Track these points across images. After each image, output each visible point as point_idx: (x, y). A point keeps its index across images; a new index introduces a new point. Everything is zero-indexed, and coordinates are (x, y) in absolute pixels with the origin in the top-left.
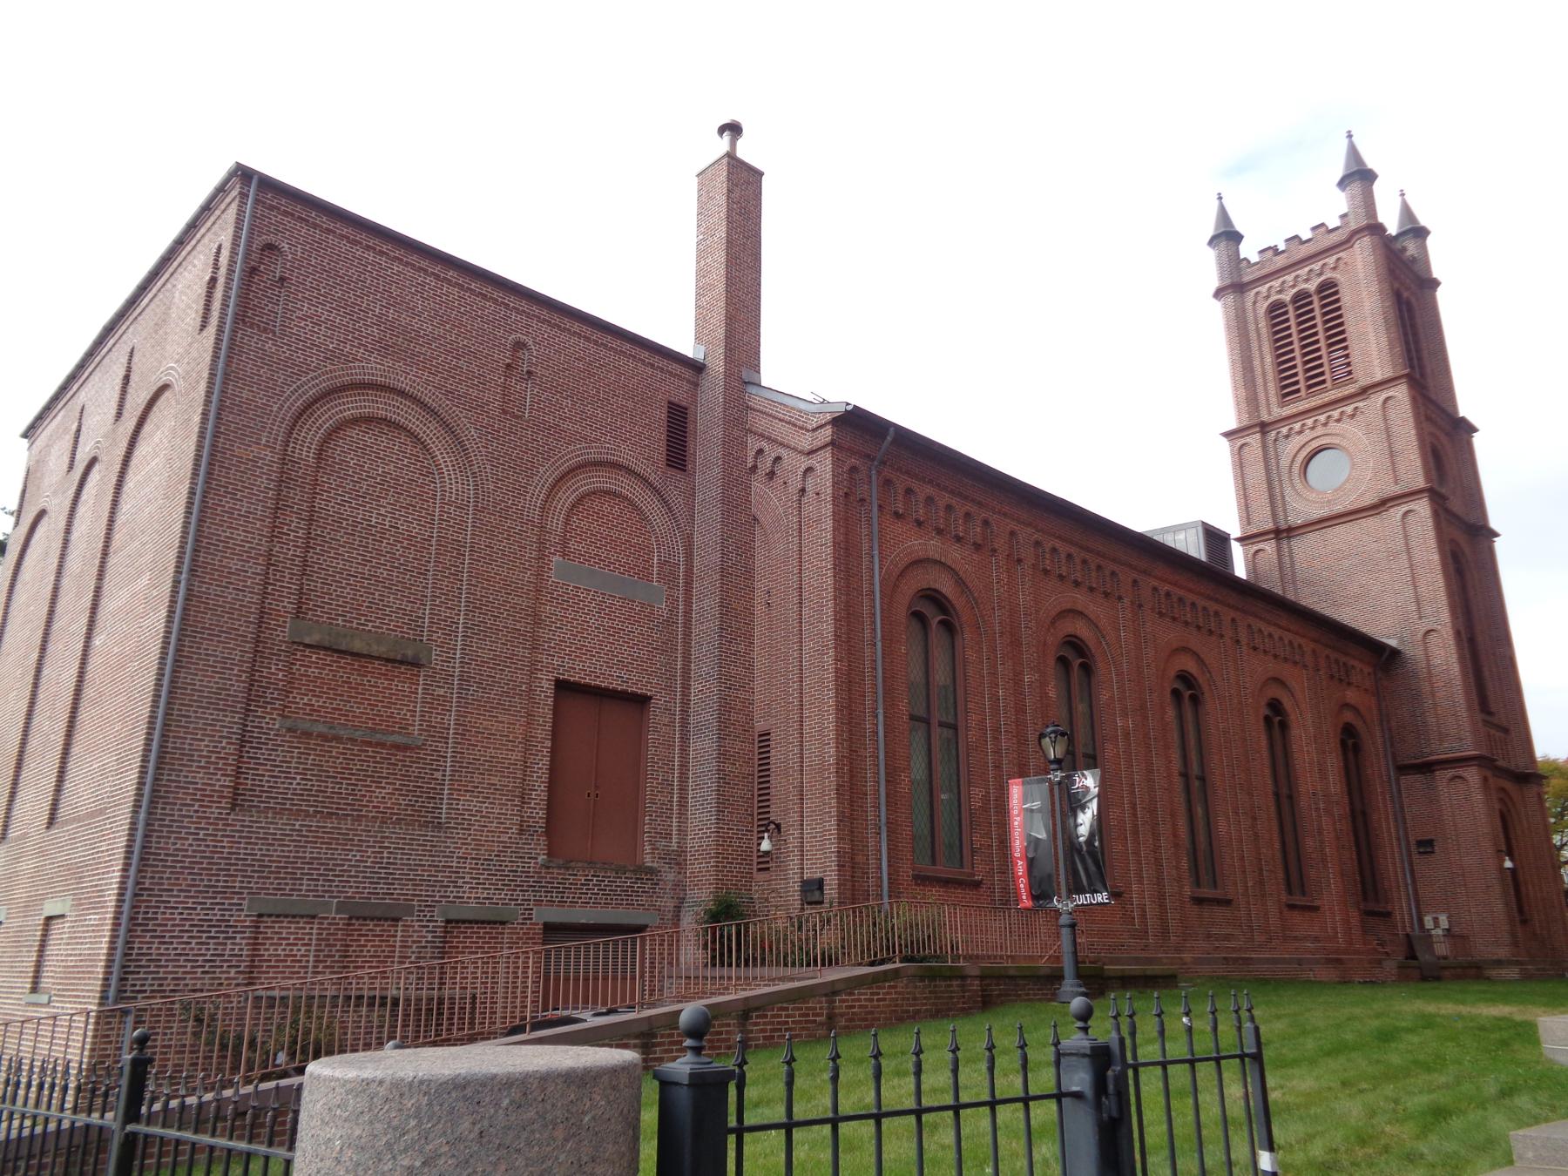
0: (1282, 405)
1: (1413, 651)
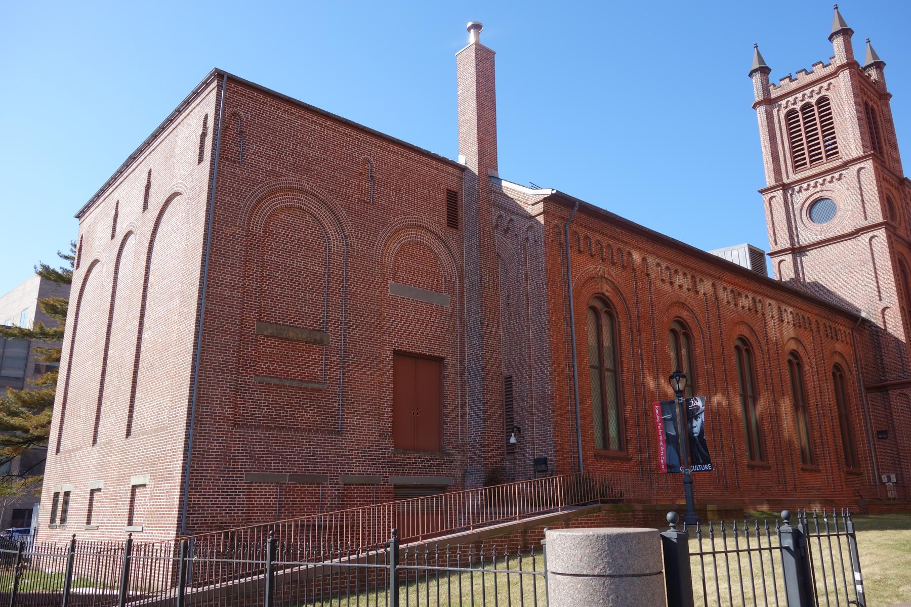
0: (795, 172)
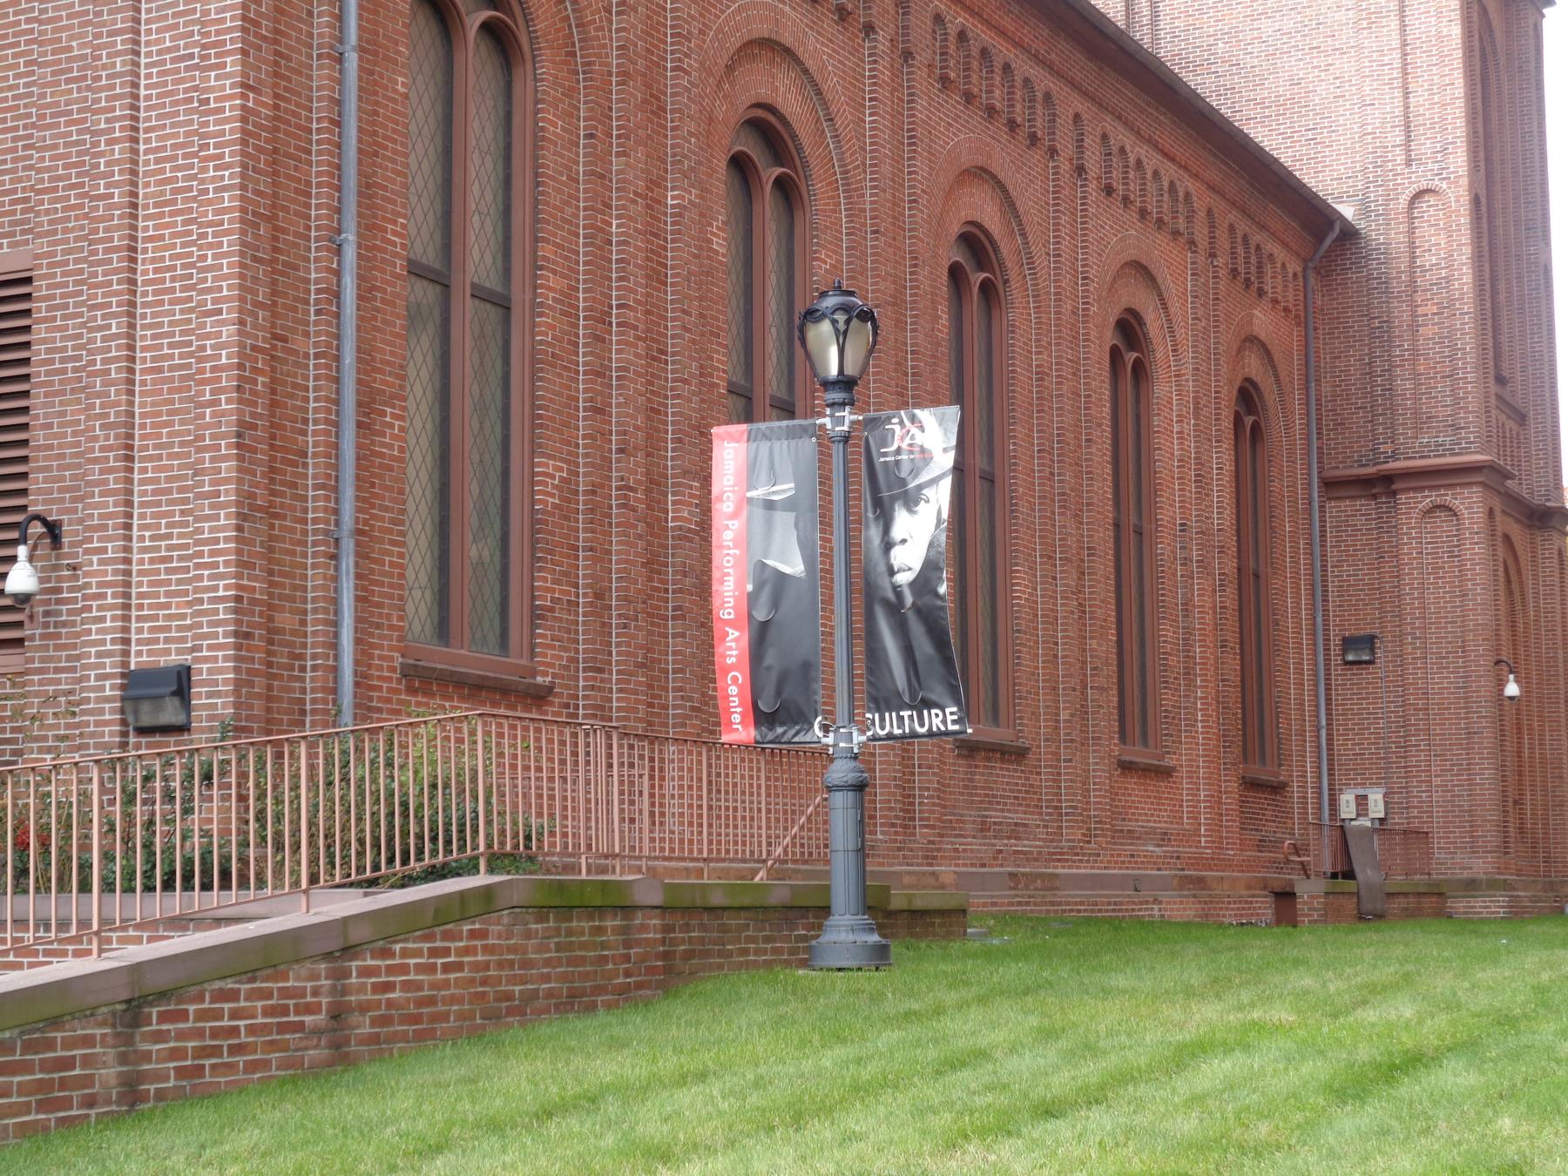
1: (1383, 235)
